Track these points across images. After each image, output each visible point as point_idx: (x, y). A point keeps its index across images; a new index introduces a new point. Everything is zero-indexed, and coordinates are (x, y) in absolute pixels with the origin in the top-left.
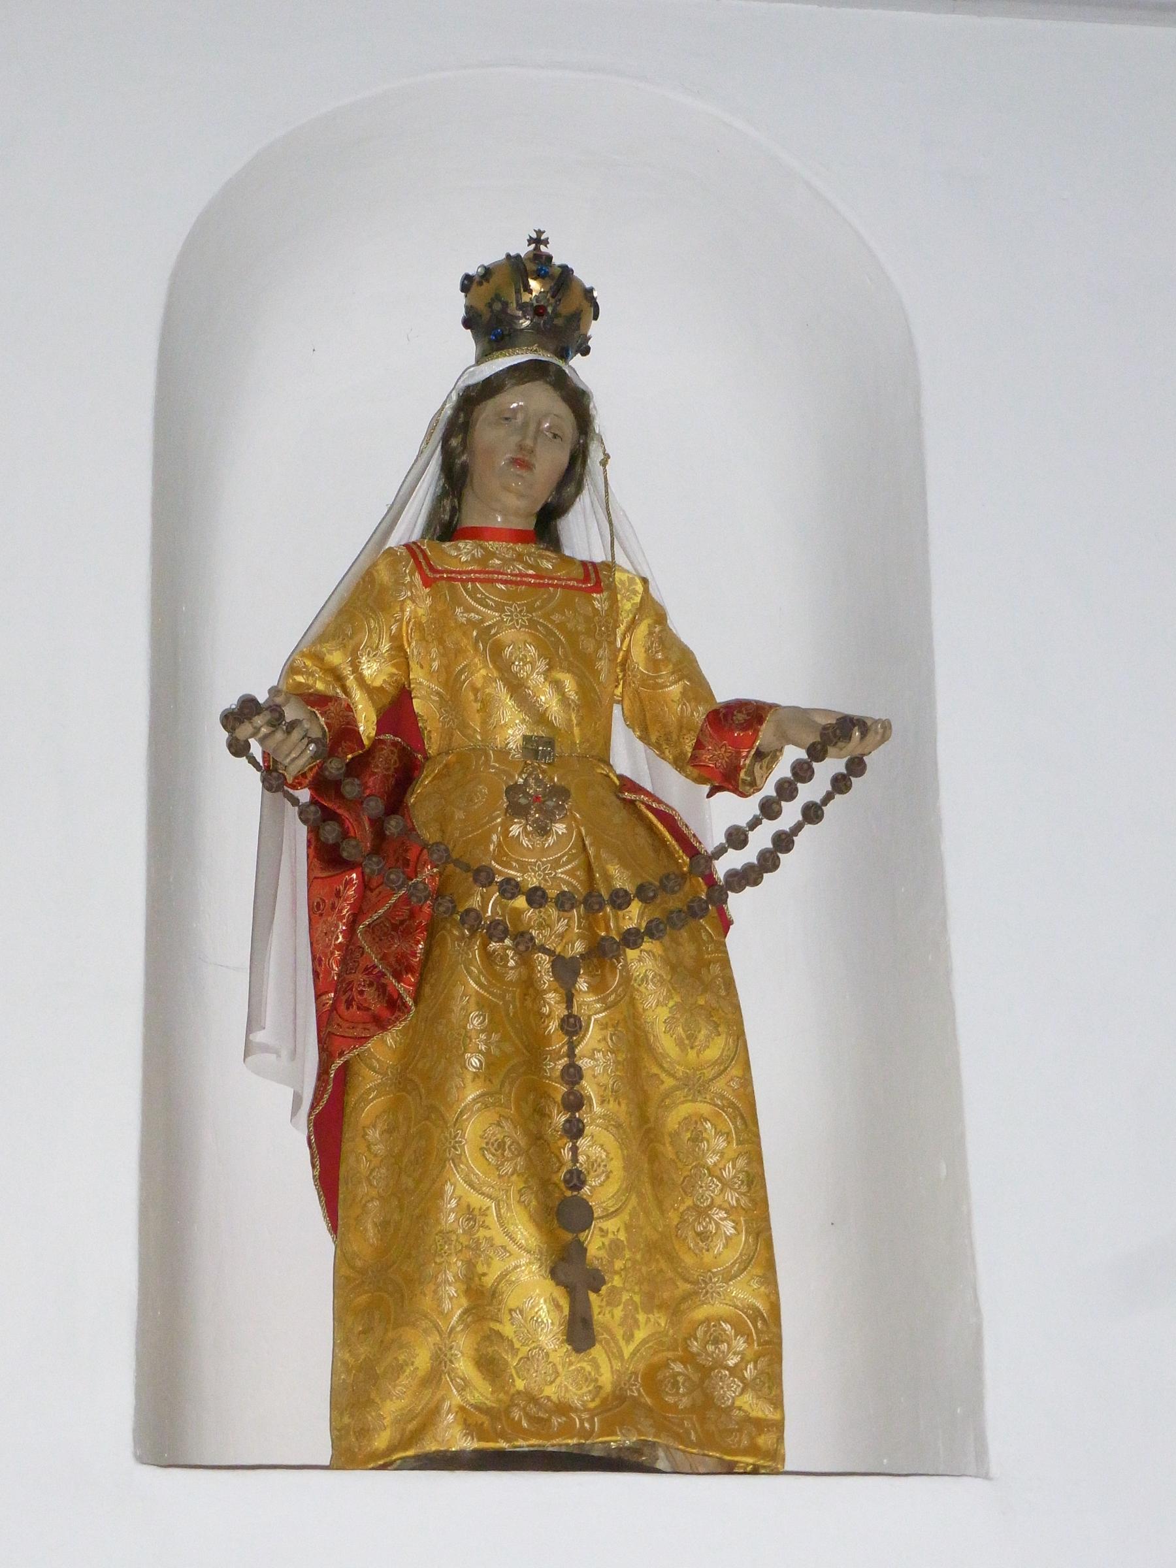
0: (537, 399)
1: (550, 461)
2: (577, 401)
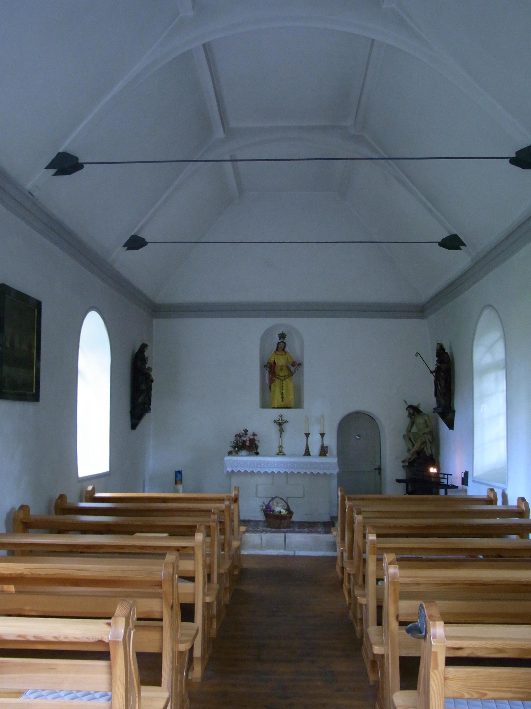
0: (282, 344)
1: (283, 347)
2: (285, 343)
